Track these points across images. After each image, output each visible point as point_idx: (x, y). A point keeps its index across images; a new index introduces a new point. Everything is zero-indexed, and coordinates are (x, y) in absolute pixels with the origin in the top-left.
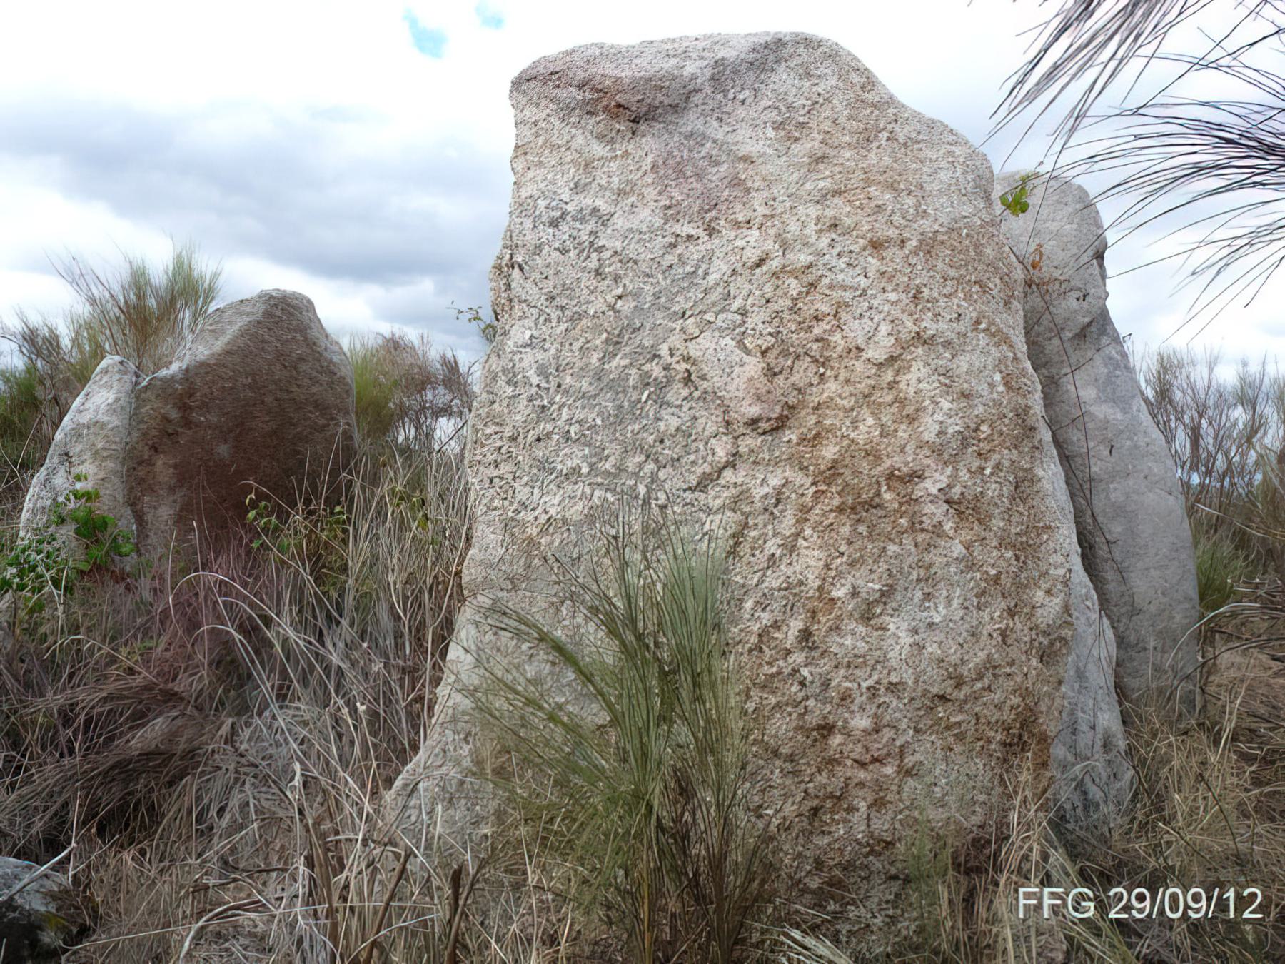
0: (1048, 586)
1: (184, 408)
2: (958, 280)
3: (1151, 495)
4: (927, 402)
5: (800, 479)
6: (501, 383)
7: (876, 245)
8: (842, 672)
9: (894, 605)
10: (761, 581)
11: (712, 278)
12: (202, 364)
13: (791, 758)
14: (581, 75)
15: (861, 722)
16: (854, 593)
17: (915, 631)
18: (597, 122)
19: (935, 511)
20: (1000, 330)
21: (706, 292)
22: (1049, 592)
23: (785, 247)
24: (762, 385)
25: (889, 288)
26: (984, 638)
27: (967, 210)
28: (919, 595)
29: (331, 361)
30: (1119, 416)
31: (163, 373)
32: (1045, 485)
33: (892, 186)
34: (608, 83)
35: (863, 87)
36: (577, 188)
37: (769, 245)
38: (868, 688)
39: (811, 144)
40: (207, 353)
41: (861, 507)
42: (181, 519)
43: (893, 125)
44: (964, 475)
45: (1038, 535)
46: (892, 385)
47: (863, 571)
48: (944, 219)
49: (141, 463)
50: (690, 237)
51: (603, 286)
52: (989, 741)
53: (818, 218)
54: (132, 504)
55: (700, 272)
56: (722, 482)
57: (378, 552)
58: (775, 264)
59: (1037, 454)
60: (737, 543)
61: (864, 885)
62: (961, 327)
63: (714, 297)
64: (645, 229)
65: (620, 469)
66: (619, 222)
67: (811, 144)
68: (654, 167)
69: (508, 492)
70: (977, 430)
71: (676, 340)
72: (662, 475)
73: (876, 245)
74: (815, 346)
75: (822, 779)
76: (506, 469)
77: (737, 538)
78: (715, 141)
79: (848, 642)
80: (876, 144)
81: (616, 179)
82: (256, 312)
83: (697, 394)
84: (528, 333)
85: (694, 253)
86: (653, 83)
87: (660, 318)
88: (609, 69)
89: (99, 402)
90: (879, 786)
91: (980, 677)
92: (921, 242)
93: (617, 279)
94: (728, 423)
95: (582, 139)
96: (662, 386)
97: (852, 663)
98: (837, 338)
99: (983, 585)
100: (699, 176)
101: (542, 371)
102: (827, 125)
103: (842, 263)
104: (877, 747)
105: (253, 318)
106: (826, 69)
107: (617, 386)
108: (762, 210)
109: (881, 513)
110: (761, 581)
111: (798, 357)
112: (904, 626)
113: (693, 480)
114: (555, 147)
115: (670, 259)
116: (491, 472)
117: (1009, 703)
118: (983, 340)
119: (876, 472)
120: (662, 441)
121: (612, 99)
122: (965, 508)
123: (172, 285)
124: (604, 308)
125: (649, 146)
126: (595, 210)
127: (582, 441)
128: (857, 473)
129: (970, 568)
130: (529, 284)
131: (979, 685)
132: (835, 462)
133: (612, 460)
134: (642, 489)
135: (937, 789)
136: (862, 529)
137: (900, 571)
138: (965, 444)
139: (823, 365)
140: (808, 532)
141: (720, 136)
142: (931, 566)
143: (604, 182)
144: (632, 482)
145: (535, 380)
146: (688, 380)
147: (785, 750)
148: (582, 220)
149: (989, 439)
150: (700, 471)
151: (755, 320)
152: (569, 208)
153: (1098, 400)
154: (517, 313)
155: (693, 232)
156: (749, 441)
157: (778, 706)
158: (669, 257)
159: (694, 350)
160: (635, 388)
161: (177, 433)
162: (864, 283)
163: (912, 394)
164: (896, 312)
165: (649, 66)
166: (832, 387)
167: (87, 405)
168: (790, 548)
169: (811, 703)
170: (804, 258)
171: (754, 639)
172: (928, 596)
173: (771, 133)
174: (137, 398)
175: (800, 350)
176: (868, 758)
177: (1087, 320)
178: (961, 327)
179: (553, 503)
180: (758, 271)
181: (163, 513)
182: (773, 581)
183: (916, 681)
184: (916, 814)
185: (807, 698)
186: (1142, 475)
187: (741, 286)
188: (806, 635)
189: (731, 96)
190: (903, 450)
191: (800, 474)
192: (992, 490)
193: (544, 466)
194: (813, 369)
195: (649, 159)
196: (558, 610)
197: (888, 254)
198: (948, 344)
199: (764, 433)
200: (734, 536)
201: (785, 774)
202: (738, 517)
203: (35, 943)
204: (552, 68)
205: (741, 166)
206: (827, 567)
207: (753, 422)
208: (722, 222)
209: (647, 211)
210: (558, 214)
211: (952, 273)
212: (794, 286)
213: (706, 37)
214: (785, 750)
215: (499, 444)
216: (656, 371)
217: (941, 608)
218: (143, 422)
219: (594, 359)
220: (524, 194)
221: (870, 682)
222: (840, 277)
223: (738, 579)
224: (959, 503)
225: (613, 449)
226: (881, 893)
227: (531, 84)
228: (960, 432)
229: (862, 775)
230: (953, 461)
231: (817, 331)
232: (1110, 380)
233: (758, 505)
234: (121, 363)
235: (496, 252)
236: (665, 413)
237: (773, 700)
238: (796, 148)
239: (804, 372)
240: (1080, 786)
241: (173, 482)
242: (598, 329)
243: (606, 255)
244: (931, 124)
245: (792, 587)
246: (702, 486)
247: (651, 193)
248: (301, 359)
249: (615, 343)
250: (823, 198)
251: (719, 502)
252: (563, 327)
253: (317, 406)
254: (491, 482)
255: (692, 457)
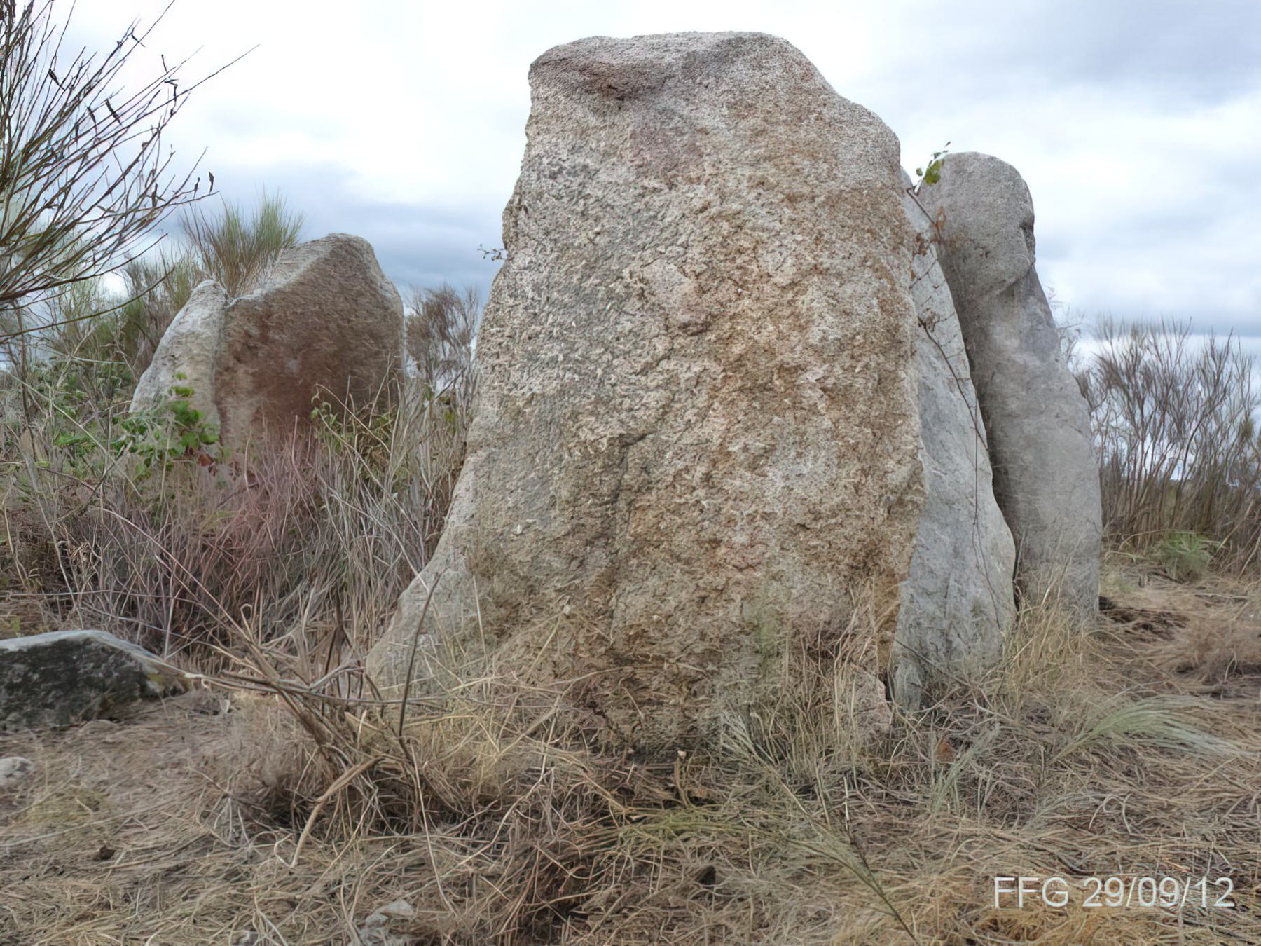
0: (899, 457)
1: (264, 327)
2: (854, 229)
3: (1061, 431)
4: (816, 316)
5: (714, 367)
6: (506, 295)
7: (792, 199)
8: (731, 502)
9: (774, 459)
10: (679, 439)
11: (668, 220)
12: (279, 291)
13: (688, 562)
14: (583, 62)
15: (740, 539)
16: (745, 449)
17: (787, 478)
18: (594, 99)
19: (812, 396)
20: (883, 268)
21: (662, 231)
22: (899, 462)
23: (723, 198)
24: (693, 299)
25: (797, 231)
26: (840, 489)
27: (871, 176)
28: (793, 453)
29: (384, 297)
30: (1038, 363)
31: (248, 297)
32: (905, 384)
33: (813, 156)
34: (603, 69)
35: (802, 75)
36: (574, 150)
37: (711, 197)
38: (749, 515)
39: (753, 122)
40: (284, 282)
41: (756, 389)
42: (256, 419)
43: (822, 108)
44: (838, 371)
45: (895, 420)
46: (790, 303)
47: (754, 434)
48: (851, 183)
49: (227, 369)
50: (655, 189)
51: (586, 224)
52: (838, 563)
53: (750, 178)
54: (218, 402)
55: (659, 216)
56: (659, 369)
57: (413, 447)
58: (713, 211)
59: (902, 361)
60: (665, 413)
61: (736, 655)
62: (850, 263)
63: (665, 235)
64: (621, 182)
65: (586, 358)
66: (603, 177)
67: (753, 122)
68: (633, 135)
69: (505, 376)
70: (853, 338)
71: (635, 266)
72: (615, 362)
73: (792, 199)
74: (737, 273)
75: (709, 578)
76: (504, 359)
77: (666, 409)
78: (681, 116)
79: (738, 483)
80: (806, 122)
81: (602, 144)
82: (325, 251)
83: (646, 307)
84: (528, 259)
85: (657, 201)
86: (638, 70)
87: (627, 250)
88: (606, 58)
89: (196, 318)
90: (750, 586)
91: (835, 515)
92: (828, 198)
93: (597, 219)
94: (667, 328)
95: (581, 113)
96: (622, 300)
97: (739, 498)
98: (753, 267)
99: (843, 450)
100: (666, 143)
101: (536, 288)
102: (769, 107)
103: (763, 212)
104: (751, 558)
105: (321, 255)
106: (775, 63)
107: (589, 299)
108: (710, 170)
109: (771, 393)
110: (679, 439)
111: (723, 280)
112: (780, 473)
113: (638, 368)
114: (559, 118)
115: (638, 205)
116: (494, 361)
117: (857, 537)
118: (867, 274)
119: (770, 365)
120: (618, 339)
121: (593, 83)
122: (836, 395)
123: (259, 234)
124: (587, 241)
125: (631, 119)
126: (585, 167)
127: (561, 338)
128: (756, 364)
129: (833, 438)
130: (531, 223)
131: (833, 521)
132: (741, 355)
133: (580, 351)
134: (599, 372)
135: (794, 591)
136: (756, 404)
137: (781, 435)
138: (841, 349)
139: (741, 287)
140: (716, 405)
141: (686, 113)
142: (804, 433)
143: (594, 146)
144: (592, 368)
145: (530, 294)
146: (641, 296)
147: (684, 556)
148: (575, 175)
149: (862, 346)
150: (643, 361)
151: (694, 252)
152: (566, 165)
153: (1020, 349)
154: (521, 244)
155: (656, 185)
156: (681, 340)
157: (682, 525)
158: (637, 204)
159: (647, 273)
160: (602, 300)
161: (256, 347)
162: (778, 226)
163: (804, 310)
164: (800, 249)
165: (636, 56)
166: (746, 302)
167: (187, 318)
168: (703, 416)
169: (706, 523)
170: (736, 206)
171: (670, 479)
172: (800, 455)
173: (725, 111)
174: (226, 315)
175: (725, 275)
176: (743, 565)
177: (1013, 280)
178: (850, 263)
179: (536, 385)
180: (700, 216)
181: (241, 412)
182: (688, 439)
183: (784, 513)
184: (777, 607)
185: (703, 520)
186: (1053, 415)
187: (687, 225)
188: (707, 477)
189: (698, 81)
190: (792, 350)
191: (714, 364)
192: (859, 383)
193: (532, 357)
194: (734, 288)
195: (630, 128)
196: (533, 460)
197: (800, 206)
198: (839, 275)
199: (692, 335)
200: (663, 407)
201: (684, 572)
202: (668, 394)
203: (143, 688)
204: (562, 55)
205: (699, 136)
206: (728, 430)
207: (684, 327)
208: (680, 179)
209: (624, 169)
210: (556, 169)
211: (850, 222)
212: (725, 226)
213: (685, 34)
214: (684, 556)
215: (500, 340)
216: (620, 289)
217: (809, 464)
218: (229, 335)
219: (576, 278)
220: (533, 153)
221: (750, 511)
222: (761, 221)
223: (663, 437)
224: (832, 390)
225: (582, 344)
226: (748, 660)
227: (545, 67)
228: (839, 340)
229: (739, 576)
230: (832, 360)
231: (739, 261)
232: (1032, 332)
233: (683, 386)
234: (215, 286)
235: (509, 198)
236: (623, 319)
237: (680, 521)
238: (743, 124)
239: (726, 291)
240: (944, 634)
241: (250, 388)
242: (579, 257)
243: (592, 200)
244: (854, 108)
245: (703, 444)
246: (644, 371)
247: (628, 155)
248: (361, 294)
249: (591, 268)
250: (756, 163)
251: (654, 383)
252: (554, 255)
253: (372, 335)
254: (493, 369)
255: (639, 351)
